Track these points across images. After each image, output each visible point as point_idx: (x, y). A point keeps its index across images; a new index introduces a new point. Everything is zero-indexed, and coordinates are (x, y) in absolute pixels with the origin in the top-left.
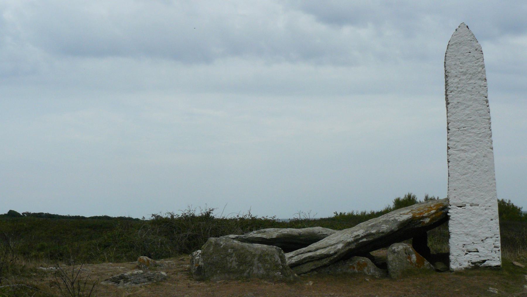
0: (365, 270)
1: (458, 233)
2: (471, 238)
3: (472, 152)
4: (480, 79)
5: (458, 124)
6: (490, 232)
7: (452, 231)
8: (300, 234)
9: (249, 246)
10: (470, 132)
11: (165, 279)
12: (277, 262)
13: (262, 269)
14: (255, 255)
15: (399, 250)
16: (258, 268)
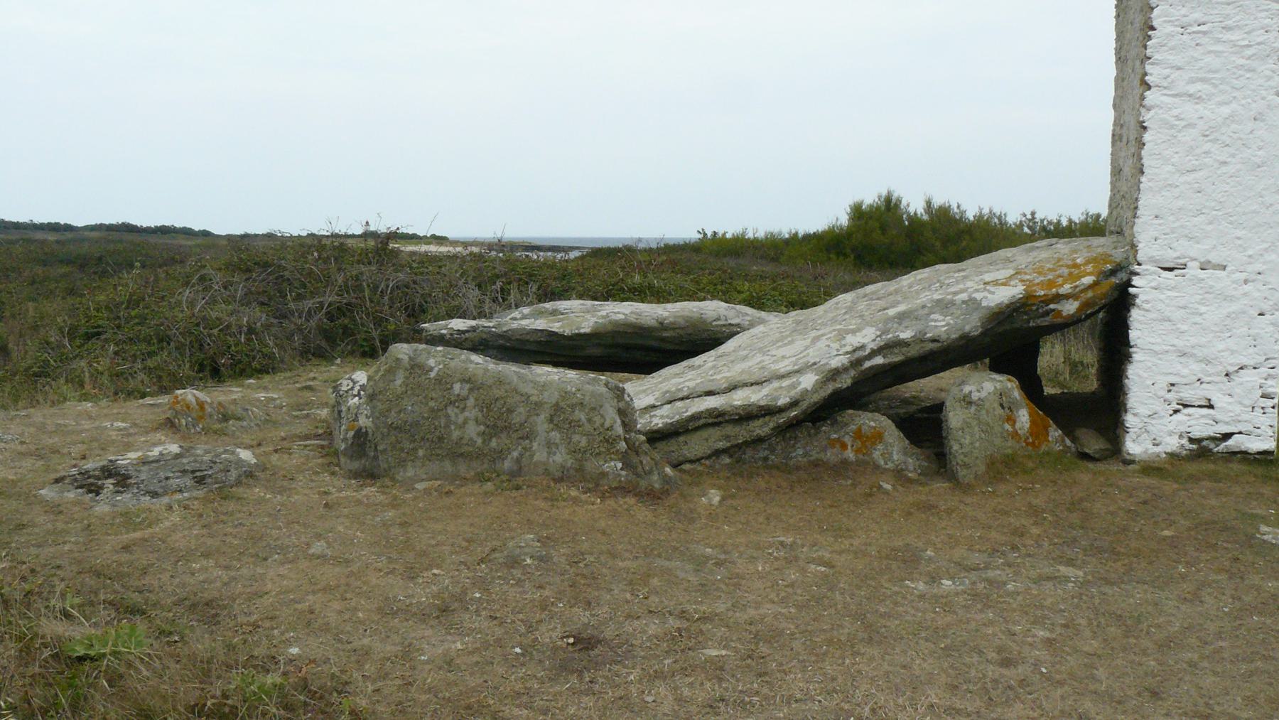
1: (1157, 348)
2: (1196, 367)
3: (1221, 104)
5: (1184, 11)
6: (1252, 350)
7: (1139, 342)
8: (661, 323)
9: (520, 376)
10: (1219, 41)
11: (249, 474)
12: (611, 428)
13: (563, 449)
14: (539, 405)
15: (983, 394)
16: (549, 445)
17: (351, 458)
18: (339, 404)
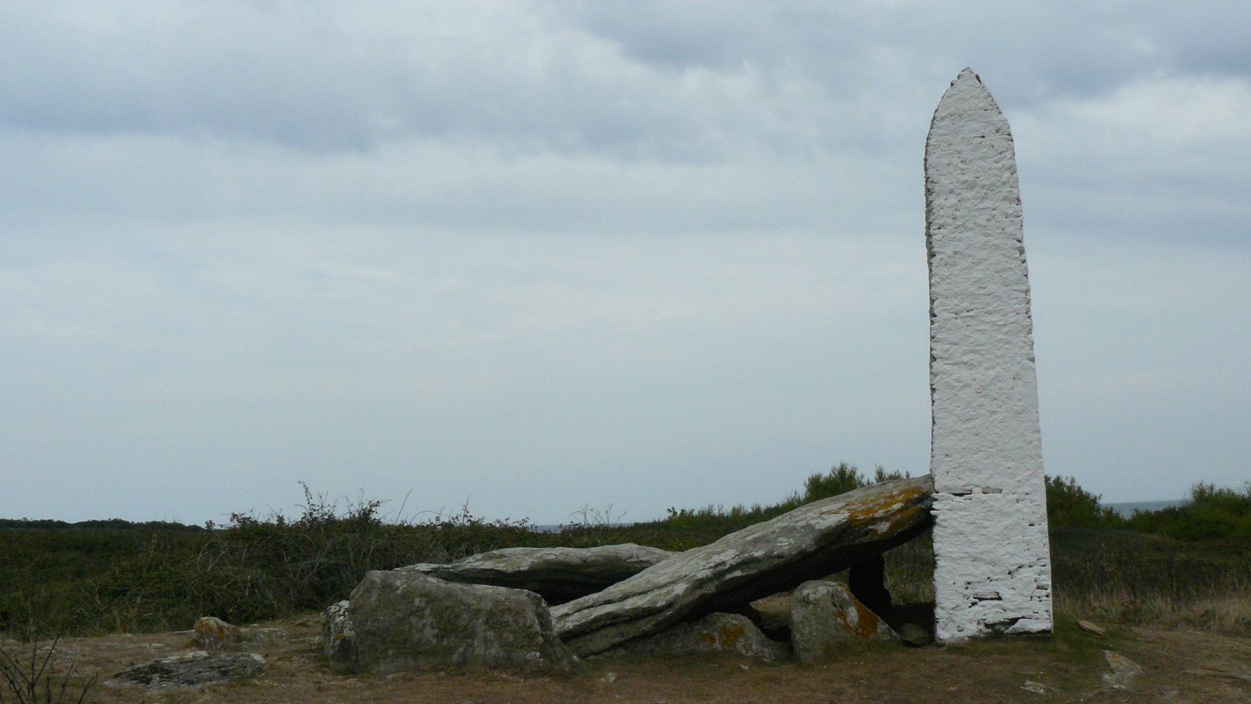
0: (739, 645)
1: (954, 556)
2: (985, 568)
3: (988, 369)
4: (1005, 199)
5: (956, 302)
6: (1026, 553)
7: (941, 552)
10: (983, 322)
11: (259, 669)
12: (531, 627)
13: (496, 645)
14: (478, 611)
15: (818, 596)
16: (486, 641)
17: (338, 661)
18: (328, 622)
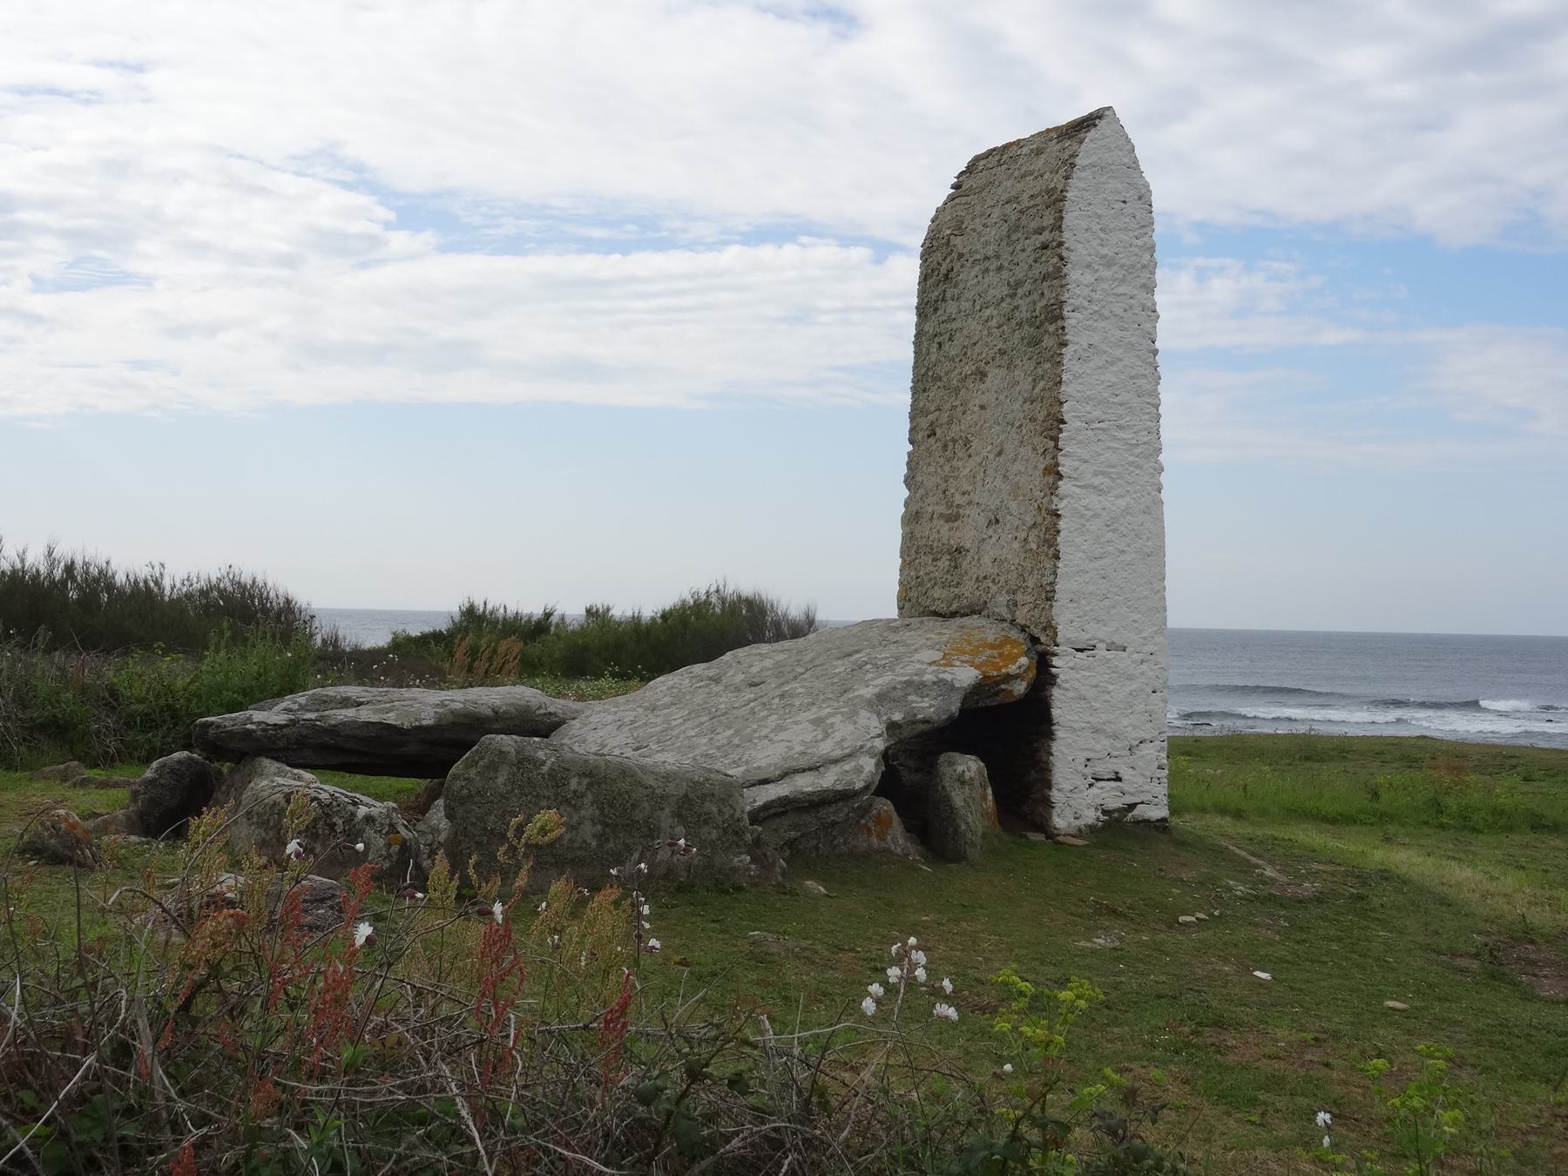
1: (1075, 725)
2: (1106, 742)
3: (1117, 497)
5: (1088, 408)
7: (1061, 720)
10: (1115, 438)
